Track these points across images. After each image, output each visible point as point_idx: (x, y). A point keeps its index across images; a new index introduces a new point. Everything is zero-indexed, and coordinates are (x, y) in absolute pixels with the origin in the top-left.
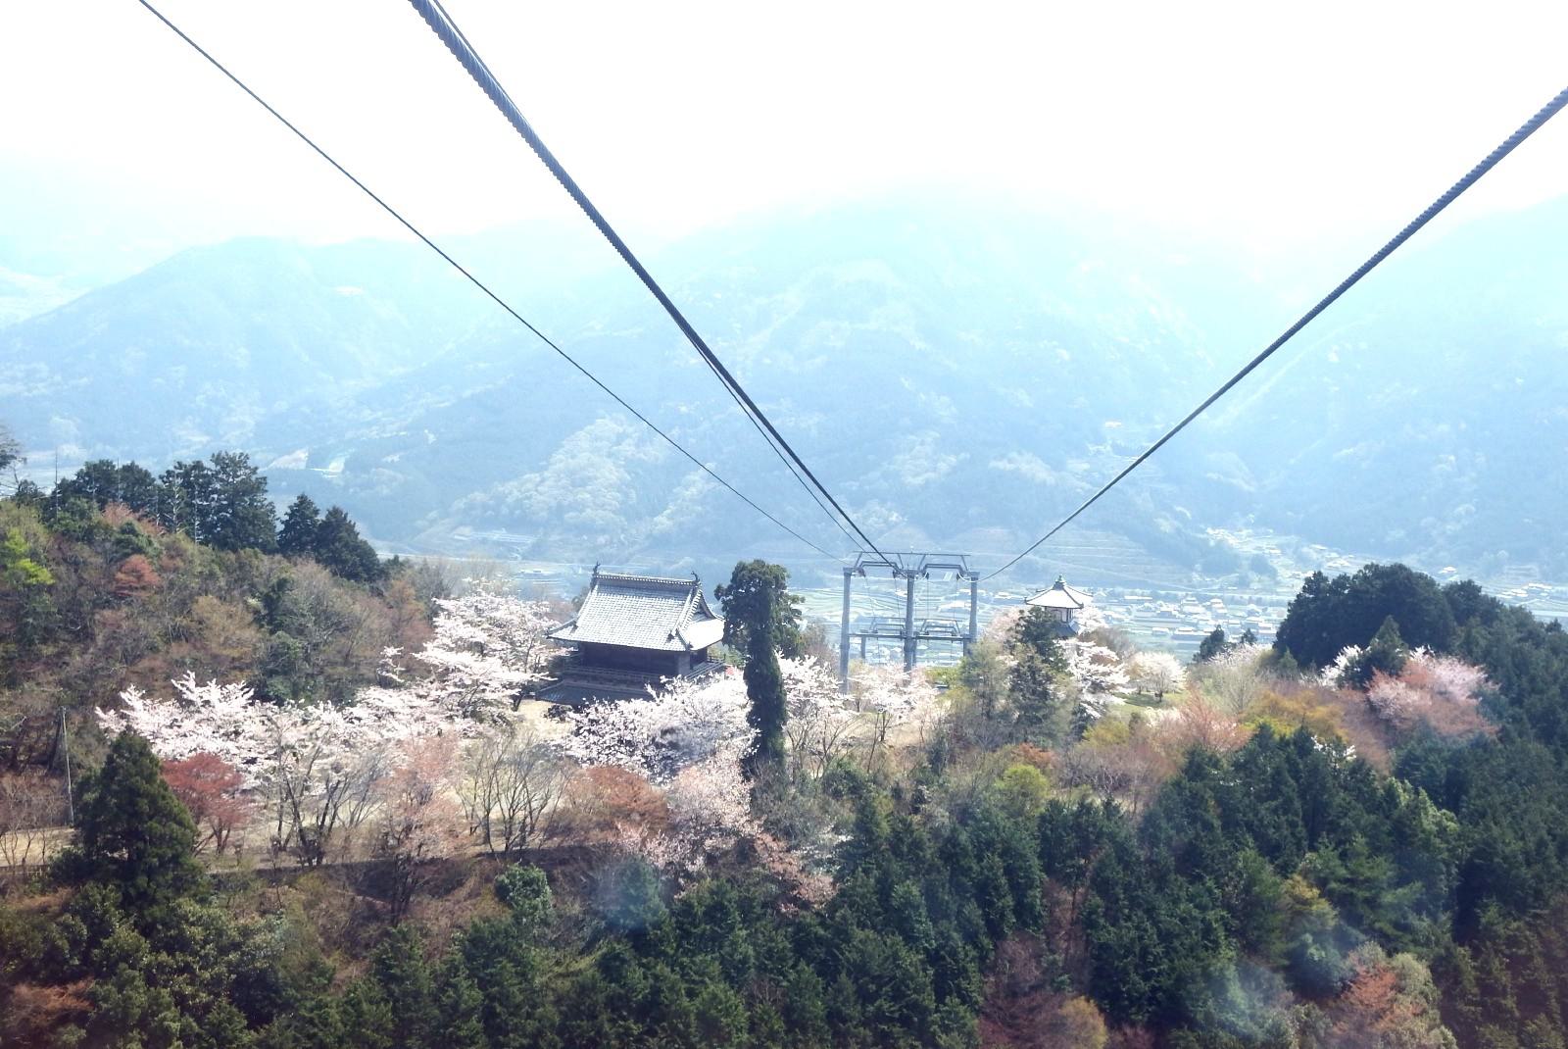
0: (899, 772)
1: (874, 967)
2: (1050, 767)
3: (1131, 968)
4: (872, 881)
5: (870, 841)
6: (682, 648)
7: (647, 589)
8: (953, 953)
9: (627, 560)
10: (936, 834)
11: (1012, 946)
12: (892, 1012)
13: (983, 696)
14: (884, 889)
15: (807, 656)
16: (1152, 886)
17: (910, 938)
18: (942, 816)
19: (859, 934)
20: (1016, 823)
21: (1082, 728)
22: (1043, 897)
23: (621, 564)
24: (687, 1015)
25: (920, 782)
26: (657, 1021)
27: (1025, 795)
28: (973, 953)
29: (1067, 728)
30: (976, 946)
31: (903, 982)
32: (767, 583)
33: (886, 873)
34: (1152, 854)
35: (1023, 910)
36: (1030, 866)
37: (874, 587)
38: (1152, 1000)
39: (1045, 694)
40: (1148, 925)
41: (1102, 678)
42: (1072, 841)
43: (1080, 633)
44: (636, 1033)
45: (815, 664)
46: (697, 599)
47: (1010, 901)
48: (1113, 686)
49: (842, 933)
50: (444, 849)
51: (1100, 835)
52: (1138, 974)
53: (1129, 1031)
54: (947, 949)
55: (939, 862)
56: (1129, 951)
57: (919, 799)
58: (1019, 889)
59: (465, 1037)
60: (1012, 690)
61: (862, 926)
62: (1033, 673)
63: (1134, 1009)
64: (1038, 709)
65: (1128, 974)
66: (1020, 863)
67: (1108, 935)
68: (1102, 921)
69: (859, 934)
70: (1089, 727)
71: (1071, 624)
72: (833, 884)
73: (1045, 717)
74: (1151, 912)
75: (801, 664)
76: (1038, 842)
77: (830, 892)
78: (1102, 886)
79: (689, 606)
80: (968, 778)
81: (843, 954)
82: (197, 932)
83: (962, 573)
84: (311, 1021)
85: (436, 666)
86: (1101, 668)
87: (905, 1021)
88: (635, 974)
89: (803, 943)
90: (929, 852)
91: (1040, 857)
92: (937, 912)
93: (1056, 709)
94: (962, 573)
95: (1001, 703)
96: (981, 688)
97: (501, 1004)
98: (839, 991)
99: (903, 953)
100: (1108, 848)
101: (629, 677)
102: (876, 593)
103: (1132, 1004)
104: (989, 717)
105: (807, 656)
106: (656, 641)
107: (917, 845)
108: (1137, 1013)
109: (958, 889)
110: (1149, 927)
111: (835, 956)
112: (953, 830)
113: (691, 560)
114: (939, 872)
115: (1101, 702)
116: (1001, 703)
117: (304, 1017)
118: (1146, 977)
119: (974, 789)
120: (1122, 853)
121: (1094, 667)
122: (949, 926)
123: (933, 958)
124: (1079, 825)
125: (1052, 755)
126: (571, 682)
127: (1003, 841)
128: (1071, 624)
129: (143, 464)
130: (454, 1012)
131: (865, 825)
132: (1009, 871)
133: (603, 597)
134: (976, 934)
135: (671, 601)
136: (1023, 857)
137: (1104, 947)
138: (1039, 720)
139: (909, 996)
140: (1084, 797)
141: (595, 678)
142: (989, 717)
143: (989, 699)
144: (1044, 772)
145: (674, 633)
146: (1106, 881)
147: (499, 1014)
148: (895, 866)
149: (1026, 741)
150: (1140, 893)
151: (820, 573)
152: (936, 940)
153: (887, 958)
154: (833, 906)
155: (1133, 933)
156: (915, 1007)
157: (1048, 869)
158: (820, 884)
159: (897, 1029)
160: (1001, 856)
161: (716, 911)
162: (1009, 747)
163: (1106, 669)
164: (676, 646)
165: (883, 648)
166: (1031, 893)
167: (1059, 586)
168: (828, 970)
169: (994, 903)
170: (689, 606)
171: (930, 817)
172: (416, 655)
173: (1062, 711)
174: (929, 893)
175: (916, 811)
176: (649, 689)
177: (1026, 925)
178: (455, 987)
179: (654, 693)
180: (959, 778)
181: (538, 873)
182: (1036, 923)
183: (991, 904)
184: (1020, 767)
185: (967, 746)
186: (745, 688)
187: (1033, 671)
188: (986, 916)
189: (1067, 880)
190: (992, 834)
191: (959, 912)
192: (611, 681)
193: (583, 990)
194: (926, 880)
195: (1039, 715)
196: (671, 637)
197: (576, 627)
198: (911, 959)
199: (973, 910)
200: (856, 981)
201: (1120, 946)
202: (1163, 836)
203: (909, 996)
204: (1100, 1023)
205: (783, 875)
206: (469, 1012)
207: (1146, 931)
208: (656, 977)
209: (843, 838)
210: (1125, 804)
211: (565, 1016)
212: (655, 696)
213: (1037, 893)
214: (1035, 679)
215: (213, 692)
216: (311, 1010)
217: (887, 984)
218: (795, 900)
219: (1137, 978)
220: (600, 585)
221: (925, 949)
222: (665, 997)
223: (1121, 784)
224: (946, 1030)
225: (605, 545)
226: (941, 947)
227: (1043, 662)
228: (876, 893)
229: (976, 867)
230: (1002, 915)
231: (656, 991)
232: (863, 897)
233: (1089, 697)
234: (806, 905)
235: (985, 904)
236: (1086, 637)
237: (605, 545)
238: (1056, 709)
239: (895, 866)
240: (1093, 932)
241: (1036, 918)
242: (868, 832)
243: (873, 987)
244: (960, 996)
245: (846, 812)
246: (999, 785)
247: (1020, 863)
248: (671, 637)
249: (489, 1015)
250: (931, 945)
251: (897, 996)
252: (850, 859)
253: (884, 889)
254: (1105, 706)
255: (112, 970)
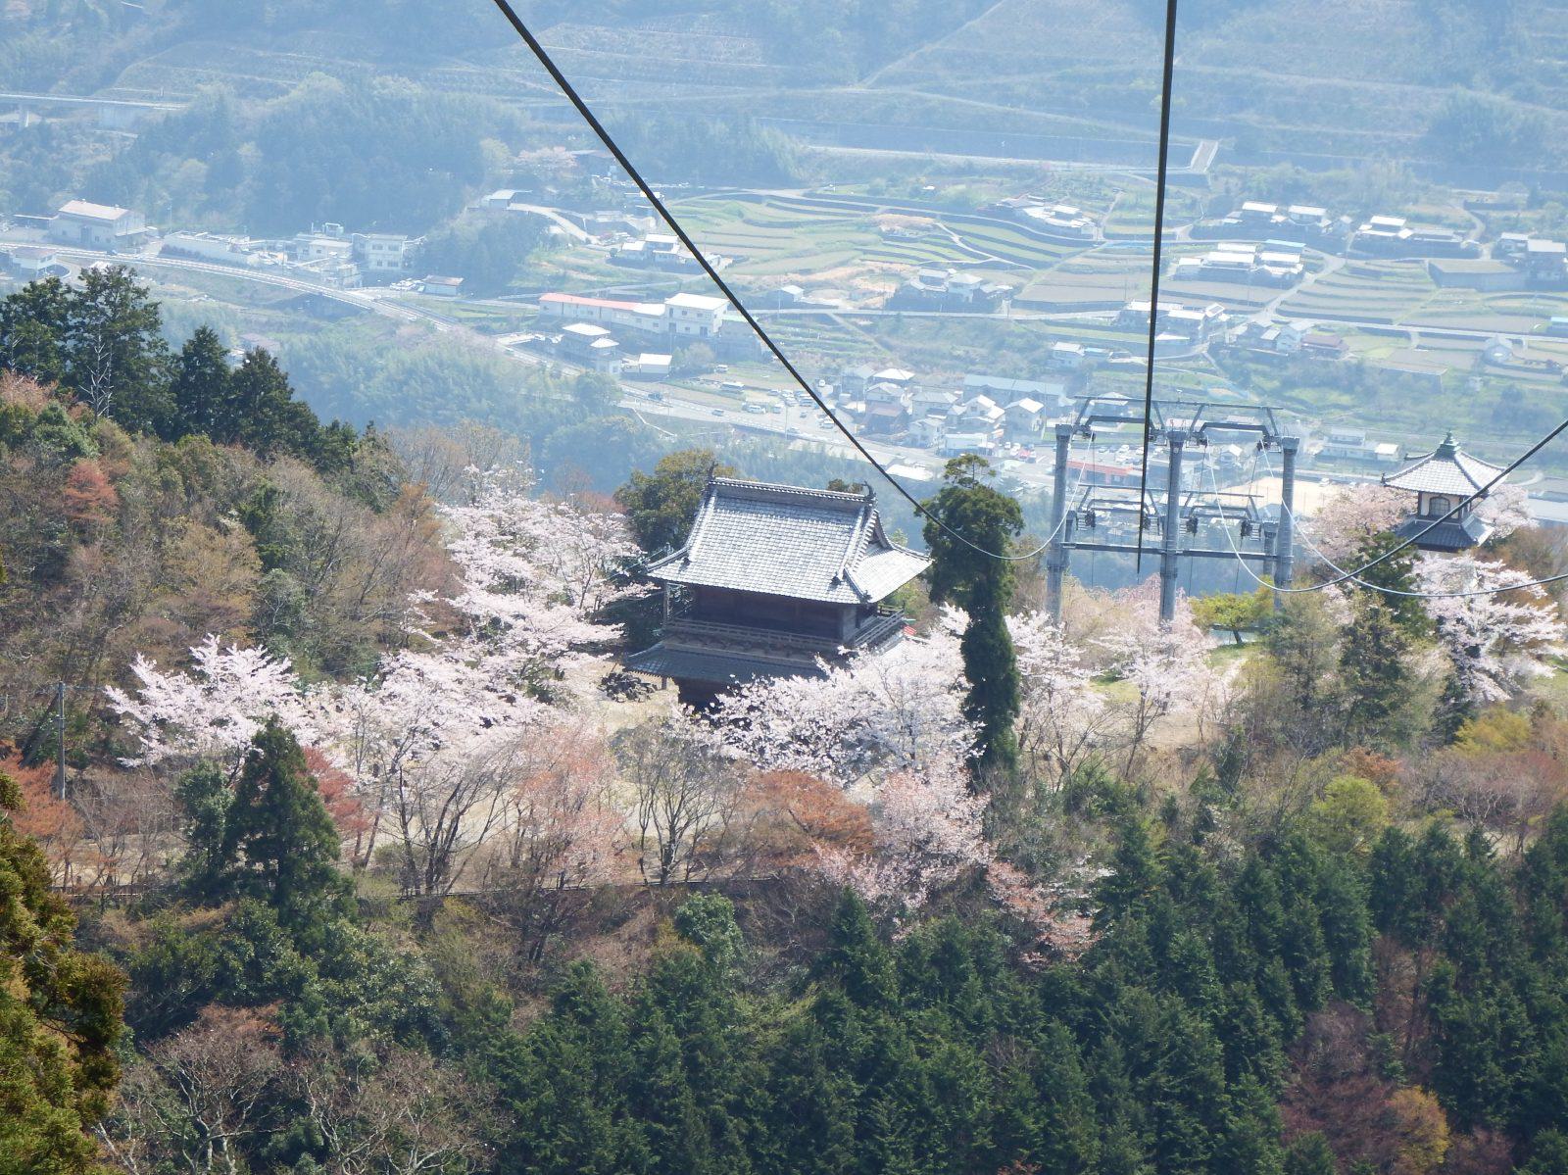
0: (1174, 785)
1: (1150, 1030)
2: (1394, 782)
3: (1488, 1055)
4: (1144, 928)
5: (1138, 876)
6: (855, 600)
7: (792, 505)
8: (1250, 1021)
9: (108, 78)
10: (1227, 871)
11: (1329, 1020)
12: (1173, 1087)
13: (1299, 670)
14: (1159, 937)
15: (1034, 612)
16: (1526, 951)
17: (1194, 1002)
18: (1235, 850)
19: (1128, 993)
20: (1340, 859)
21: (1458, 723)
22: (1373, 958)
23: (90, 91)
24: (919, 1076)
25: (1206, 800)
26: (880, 1082)
27: (1353, 822)
28: (1276, 1025)
29: (1428, 724)
30: (1280, 1017)
31: (1184, 1051)
32: (996, 519)
33: (1162, 917)
34: (1532, 907)
35: (1345, 977)
36: (1356, 915)
37: (953, 190)
38: (1515, 1099)
39: (1395, 672)
40: (1515, 999)
41: (1517, 629)
42: (1416, 884)
43: (1481, 540)
44: (857, 1093)
45: (1047, 623)
46: (871, 521)
47: (1326, 961)
48: (1534, 644)
49: (1107, 991)
50: (606, 871)
51: (1458, 878)
52: (1498, 1064)
53: (1481, 1135)
54: (1242, 1016)
55: (1235, 906)
56: (1487, 1032)
57: (1206, 823)
58: (1341, 944)
59: (667, 1088)
60: (1345, 662)
61: (1129, 981)
62: (1377, 637)
63: (1489, 1109)
64: (1381, 695)
65: (1484, 1062)
66: (1342, 911)
67: (1457, 1010)
68: (1452, 993)
69: (1128, 993)
70: (1467, 721)
71: (1466, 524)
72: (1093, 929)
73: (1394, 706)
74: (1522, 985)
75: (1026, 623)
76: (1368, 885)
77: (1086, 940)
78: (1454, 944)
79: (860, 533)
80: (1272, 799)
81: (1108, 1015)
82: (358, 956)
83: (1268, 439)
84: (503, 1060)
85: (477, 618)
86: (1513, 611)
87: (1188, 1099)
88: (851, 1025)
89: (1054, 998)
90: (1220, 892)
91: (1371, 905)
92: (1230, 971)
93: (1410, 694)
94: (1268, 438)
95: (1326, 680)
96: (1295, 658)
97: (704, 1053)
98: (1103, 1057)
99: (1184, 1017)
100: (1467, 893)
101: (769, 640)
102: (958, 211)
103: (1488, 1102)
104: (1306, 703)
105: (1034, 612)
106: (812, 587)
107: (1201, 883)
108: (1494, 1114)
109: (1261, 944)
110: (1516, 1002)
111: (1097, 1019)
112: (1252, 866)
113: (334, 85)
114: (1234, 917)
115: (1511, 672)
116: (1326, 680)
117: (495, 1057)
118: (1509, 1068)
119: (1281, 811)
120: (1490, 910)
121: (1500, 609)
122: (1244, 988)
123: (1224, 1030)
124: (1428, 864)
125: (1402, 765)
126: (676, 644)
127: (1321, 880)
128: (1466, 524)
129: (314, 410)
130: (651, 1061)
131: (1128, 859)
132: (1327, 921)
133: (724, 515)
134: (1282, 1001)
135: (832, 527)
136: (1344, 902)
137: (1457, 1027)
138: (1384, 712)
139: (1194, 1068)
140: (1438, 824)
141: (714, 640)
142: (1306, 703)
143: (1307, 676)
144: (1383, 790)
145: (840, 577)
146: (1462, 938)
147: (703, 1065)
148: (1174, 910)
149: (1360, 743)
150: (1509, 959)
151: (771, 136)
152: (1227, 1005)
153: (1163, 1024)
154: (1090, 960)
155: (1494, 1010)
156: (1201, 1080)
157: (1381, 923)
158: (1074, 931)
159: (1176, 1108)
160: (1316, 900)
161: (947, 956)
162: (1335, 751)
163: (1521, 612)
164: (844, 596)
165: (983, 400)
166: (1355, 952)
167: (1445, 453)
168: (1088, 1034)
169: (1305, 962)
170: (860, 533)
171: (1216, 852)
172: (452, 602)
173: (1420, 698)
174: (1221, 945)
175: (1198, 840)
176: (820, 662)
177: (1347, 995)
178: (651, 1029)
179: (826, 668)
180: (1262, 796)
181: (720, 901)
182: (1361, 994)
183: (1300, 962)
184: (1347, 781)
185: (1271, 750)
186: (962, 665)
187: (1377, 633)
188: (1295, 977)
189: (1409, 941)
190: (1306, 870)
191: (1260, 972)
192: (739, 643)
193: (795, 1040)
194: (1217, 928)
195: (1384, 703)
196: (835, 582)
197: (687, 562)
198: (1196, 1025)
199: (1276, 969)
200: (1125, 1046)
201: (1477, 1025)
202: (1550, 885)
203: (1194, 1068)
204: (1443, 1128)
205: (1026, 916)
206: (668, 1061)
207: (1511, 1007)
208: (878, 1030)
209: (1105, 873)
210: (1502, 846)
211: (775, 1072)
212: (828, 672)
213: (1365, 953)
214: (1380, 647)
215: (243, 660)
216: (501, 1049)
217: (1164, 1054)
218: (1042, 947)
219: (1496, 1069)
220: (719, 496)
221: (1213, 1015)
222: (893, 1052)
223: (1501, 814)
224: (1238, 1111)
225: (32, 24)
226: (1234, 1014)
227: (1395, 620)
228: (1147, 942)
229: (1281, 917)
230: (1317, 978)
231: (880, 1048)
232: (1133, 947)
233: (1490, 663)
234: (1056, 956)
235: (1292, 963)
236: (1490, 550)
237: (32, 24)
238: (1410, 694)
239: (1174, 910)
240: (1439, 1007)
241: (1361, 987)
242: (1136, 865)
243: (1145, 1055)
244: (1257, 1072)
245: (1102, 837)
246: (1319, 806)
247: (1342, 911)
248: (835, 582)
249: (691, 1064)
250: (1220, 1011)
251: (1175, 1070)
252: (1111, 898)
253: (1159, 937)
254: (1520, 678)
255: (355, 974)
